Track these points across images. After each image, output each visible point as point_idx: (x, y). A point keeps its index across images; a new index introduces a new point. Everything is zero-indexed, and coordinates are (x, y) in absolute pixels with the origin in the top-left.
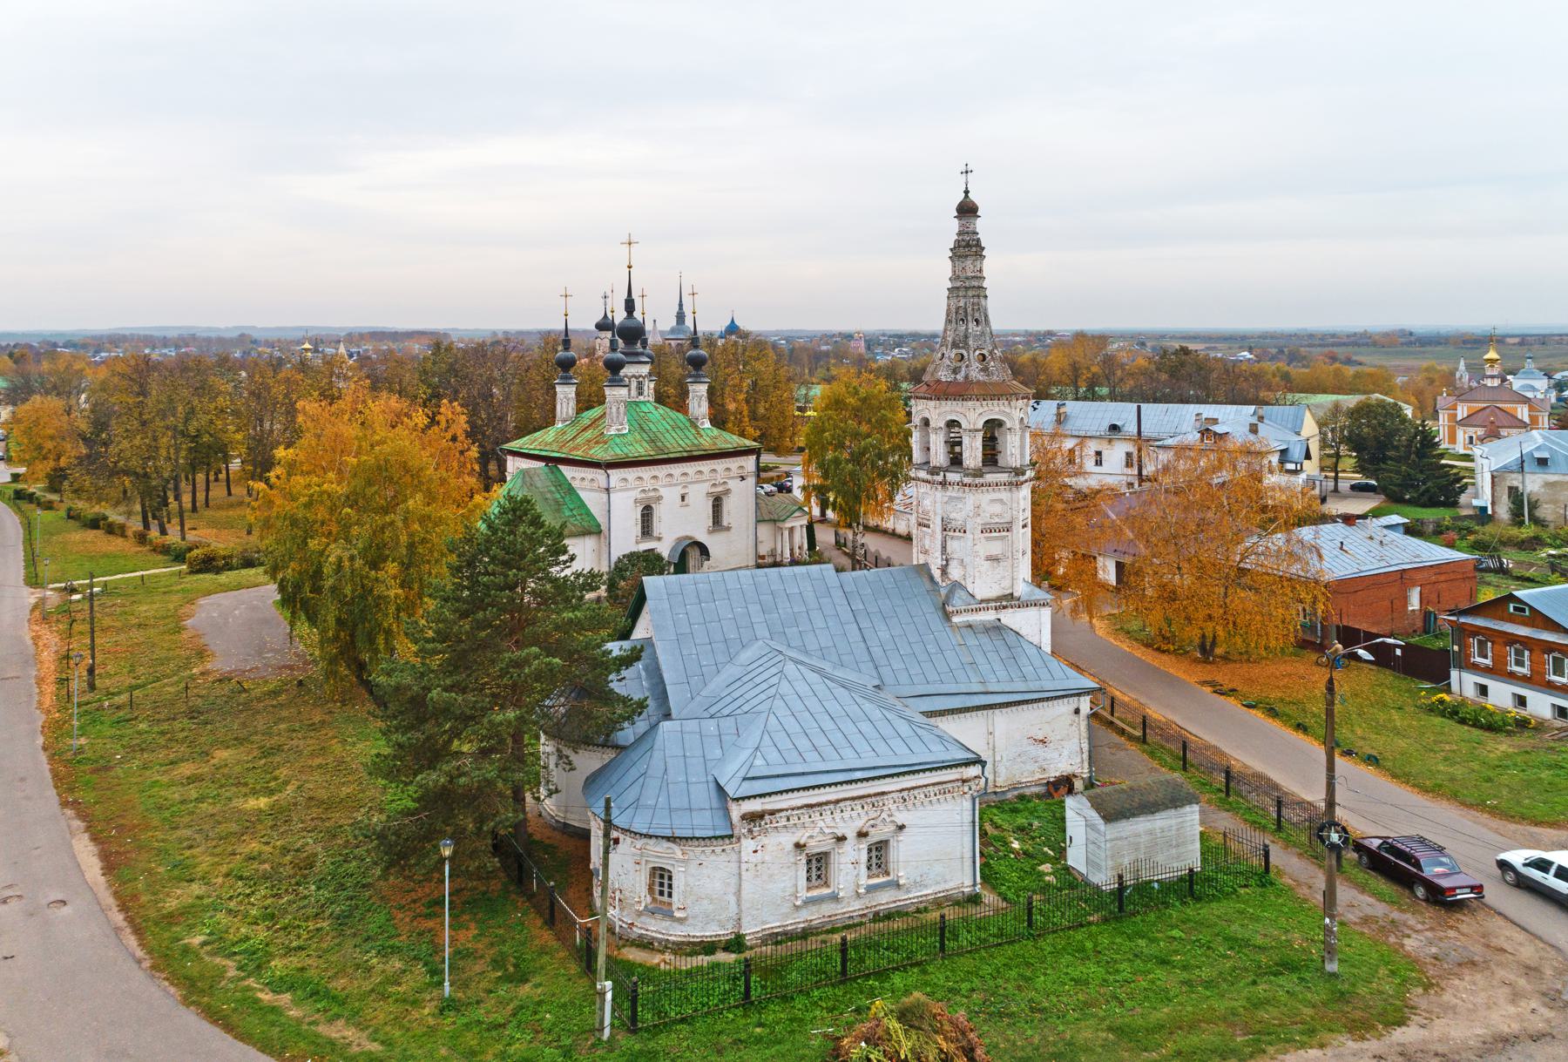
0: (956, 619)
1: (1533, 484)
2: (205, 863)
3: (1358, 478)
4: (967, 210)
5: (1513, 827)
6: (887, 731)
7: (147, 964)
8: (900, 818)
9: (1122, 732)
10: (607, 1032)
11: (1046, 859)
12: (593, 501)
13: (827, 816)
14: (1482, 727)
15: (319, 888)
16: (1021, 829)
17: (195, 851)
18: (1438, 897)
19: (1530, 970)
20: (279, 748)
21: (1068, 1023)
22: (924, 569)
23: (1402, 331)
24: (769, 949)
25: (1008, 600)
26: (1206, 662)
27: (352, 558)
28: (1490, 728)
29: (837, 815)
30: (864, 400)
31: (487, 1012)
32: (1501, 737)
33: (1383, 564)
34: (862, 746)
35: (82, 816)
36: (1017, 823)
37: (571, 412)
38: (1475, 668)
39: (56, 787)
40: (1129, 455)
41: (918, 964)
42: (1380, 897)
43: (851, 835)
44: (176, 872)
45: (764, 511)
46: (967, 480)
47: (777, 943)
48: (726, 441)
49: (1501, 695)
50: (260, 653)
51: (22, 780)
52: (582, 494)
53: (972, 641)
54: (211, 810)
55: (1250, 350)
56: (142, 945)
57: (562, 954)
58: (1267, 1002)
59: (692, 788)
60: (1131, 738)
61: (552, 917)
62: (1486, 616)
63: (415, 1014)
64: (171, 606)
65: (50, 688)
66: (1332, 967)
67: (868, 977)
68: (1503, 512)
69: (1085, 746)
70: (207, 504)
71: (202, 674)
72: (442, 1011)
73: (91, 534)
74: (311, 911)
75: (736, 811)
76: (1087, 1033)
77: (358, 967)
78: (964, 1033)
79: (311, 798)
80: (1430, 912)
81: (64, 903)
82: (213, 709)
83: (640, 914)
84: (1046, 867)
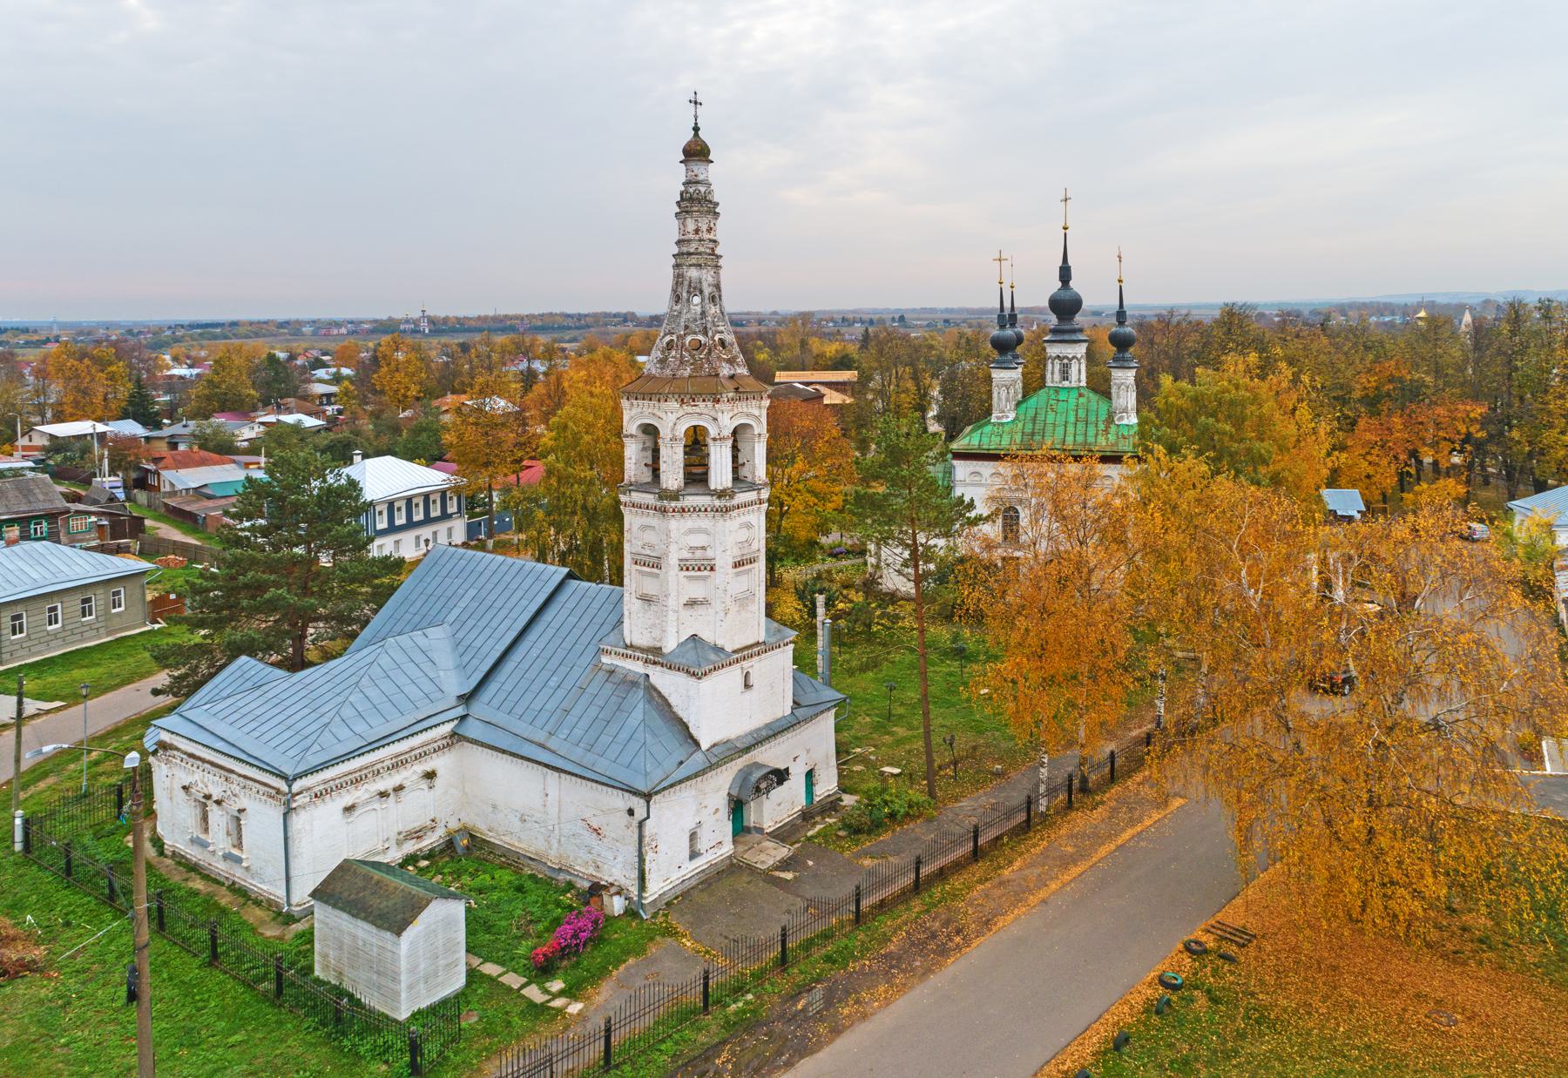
4: (696, 152)
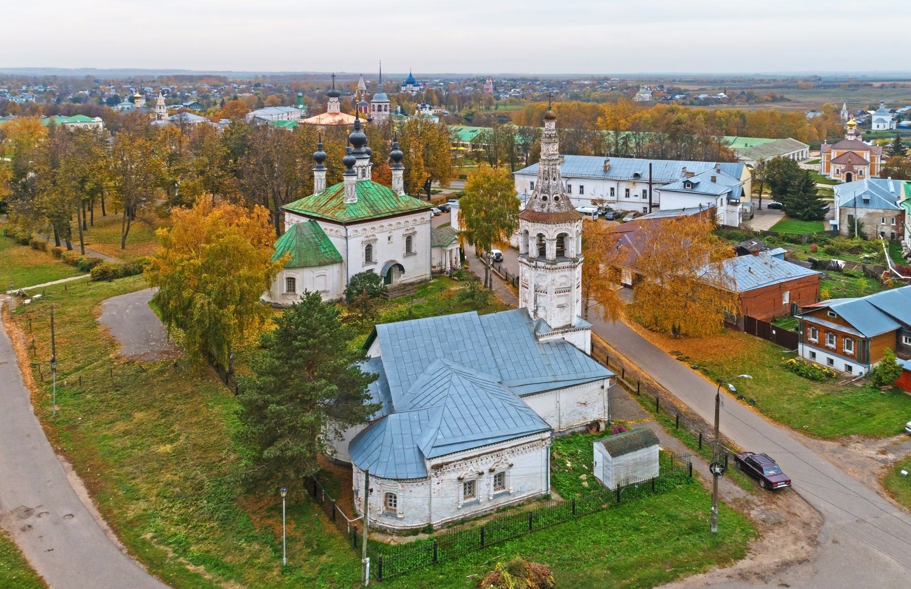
0: (541, 340)
1: (861, 214)
2: (144, 488)
3: (772, 202)
5: (813, 441)
6: (505, 414)
7: (125, 551)
8: (510, 461)
9: (627, 388)
10: (367, 582)
11: (584, 471)
12: (338, 243)
13: (475, 464)
14: (809, 378)
15: (208, 502)
16: (572, 455)
17: (138, 480)
18: (770, 487)
19: (806, 525)
20: (171, 411)
21: (590, 566)
22: (525, 311)
23: (815, 76)
24: (444, 531)
25: (568, 328)
26: (675, 338)
27: (209, 303)
28: (813, 379)
29: (479, 462)
30: (493, 185)
31: (305, 572)
32: (818, 384)
33: (771, 280)
34: (492, 424)
35: (69, 459)
36: (570, 448)
37: (323, 187)
38: (810, 344)
39: (49, 441)
40: (645, 191)
41: (519, 536)
42: (743, 487)
43: (486, 472)
44: (129, 495)
45: (436, 241)
46: (548, 266)
47: (449, 527)
48: (414, 204)
49: (822, 357)
50: (147, 341)
51: (28, 436)
52: (331, 239)
53: (549, 352)
54: (140, 454)
55: (725, 92)
56: (121, 540)
57: (341, 538)
58: (683, 549)
59: (406, 451)
60: (632, 392)
61: (334, 517)
62: (817, 317)
63: (270, 575)
64: (87, 307)
65: (28, 371)
66: (714, 530)
67: (494, 545)
68: (845, 229)
69: (606, 405)
70: (92, 225)
71: (116, 358)
72: (283, 573)
73: (24, 250)
74: (207, 516)
75: (429, 465)
76: (599, 571)
77: (236, 548)
78: (539, 576)
79: (195, 445)
80: (765, 495)
81: (72, 516)
82: (128, 384)
83: (380, 516)
84: (584, 477)
